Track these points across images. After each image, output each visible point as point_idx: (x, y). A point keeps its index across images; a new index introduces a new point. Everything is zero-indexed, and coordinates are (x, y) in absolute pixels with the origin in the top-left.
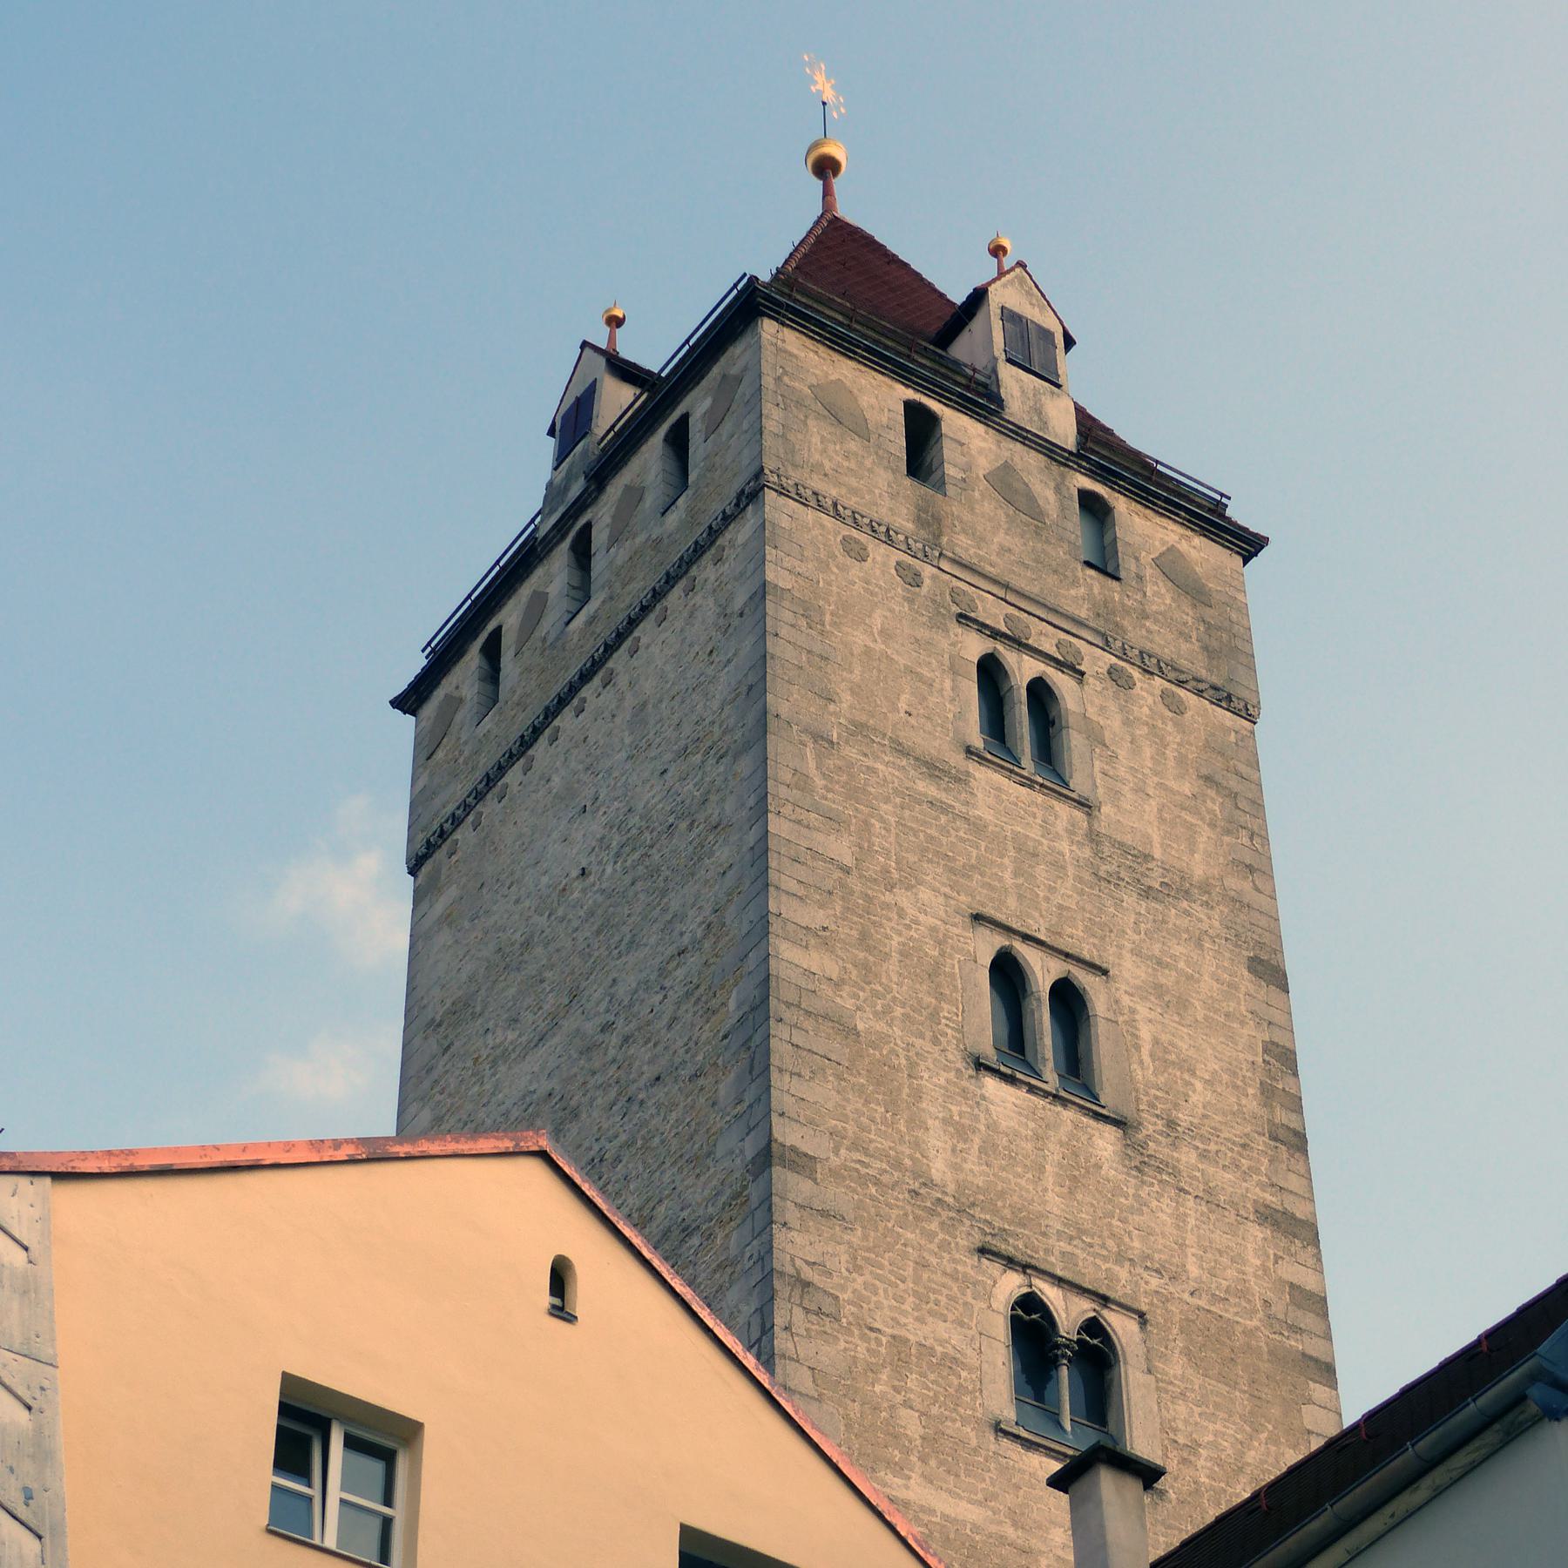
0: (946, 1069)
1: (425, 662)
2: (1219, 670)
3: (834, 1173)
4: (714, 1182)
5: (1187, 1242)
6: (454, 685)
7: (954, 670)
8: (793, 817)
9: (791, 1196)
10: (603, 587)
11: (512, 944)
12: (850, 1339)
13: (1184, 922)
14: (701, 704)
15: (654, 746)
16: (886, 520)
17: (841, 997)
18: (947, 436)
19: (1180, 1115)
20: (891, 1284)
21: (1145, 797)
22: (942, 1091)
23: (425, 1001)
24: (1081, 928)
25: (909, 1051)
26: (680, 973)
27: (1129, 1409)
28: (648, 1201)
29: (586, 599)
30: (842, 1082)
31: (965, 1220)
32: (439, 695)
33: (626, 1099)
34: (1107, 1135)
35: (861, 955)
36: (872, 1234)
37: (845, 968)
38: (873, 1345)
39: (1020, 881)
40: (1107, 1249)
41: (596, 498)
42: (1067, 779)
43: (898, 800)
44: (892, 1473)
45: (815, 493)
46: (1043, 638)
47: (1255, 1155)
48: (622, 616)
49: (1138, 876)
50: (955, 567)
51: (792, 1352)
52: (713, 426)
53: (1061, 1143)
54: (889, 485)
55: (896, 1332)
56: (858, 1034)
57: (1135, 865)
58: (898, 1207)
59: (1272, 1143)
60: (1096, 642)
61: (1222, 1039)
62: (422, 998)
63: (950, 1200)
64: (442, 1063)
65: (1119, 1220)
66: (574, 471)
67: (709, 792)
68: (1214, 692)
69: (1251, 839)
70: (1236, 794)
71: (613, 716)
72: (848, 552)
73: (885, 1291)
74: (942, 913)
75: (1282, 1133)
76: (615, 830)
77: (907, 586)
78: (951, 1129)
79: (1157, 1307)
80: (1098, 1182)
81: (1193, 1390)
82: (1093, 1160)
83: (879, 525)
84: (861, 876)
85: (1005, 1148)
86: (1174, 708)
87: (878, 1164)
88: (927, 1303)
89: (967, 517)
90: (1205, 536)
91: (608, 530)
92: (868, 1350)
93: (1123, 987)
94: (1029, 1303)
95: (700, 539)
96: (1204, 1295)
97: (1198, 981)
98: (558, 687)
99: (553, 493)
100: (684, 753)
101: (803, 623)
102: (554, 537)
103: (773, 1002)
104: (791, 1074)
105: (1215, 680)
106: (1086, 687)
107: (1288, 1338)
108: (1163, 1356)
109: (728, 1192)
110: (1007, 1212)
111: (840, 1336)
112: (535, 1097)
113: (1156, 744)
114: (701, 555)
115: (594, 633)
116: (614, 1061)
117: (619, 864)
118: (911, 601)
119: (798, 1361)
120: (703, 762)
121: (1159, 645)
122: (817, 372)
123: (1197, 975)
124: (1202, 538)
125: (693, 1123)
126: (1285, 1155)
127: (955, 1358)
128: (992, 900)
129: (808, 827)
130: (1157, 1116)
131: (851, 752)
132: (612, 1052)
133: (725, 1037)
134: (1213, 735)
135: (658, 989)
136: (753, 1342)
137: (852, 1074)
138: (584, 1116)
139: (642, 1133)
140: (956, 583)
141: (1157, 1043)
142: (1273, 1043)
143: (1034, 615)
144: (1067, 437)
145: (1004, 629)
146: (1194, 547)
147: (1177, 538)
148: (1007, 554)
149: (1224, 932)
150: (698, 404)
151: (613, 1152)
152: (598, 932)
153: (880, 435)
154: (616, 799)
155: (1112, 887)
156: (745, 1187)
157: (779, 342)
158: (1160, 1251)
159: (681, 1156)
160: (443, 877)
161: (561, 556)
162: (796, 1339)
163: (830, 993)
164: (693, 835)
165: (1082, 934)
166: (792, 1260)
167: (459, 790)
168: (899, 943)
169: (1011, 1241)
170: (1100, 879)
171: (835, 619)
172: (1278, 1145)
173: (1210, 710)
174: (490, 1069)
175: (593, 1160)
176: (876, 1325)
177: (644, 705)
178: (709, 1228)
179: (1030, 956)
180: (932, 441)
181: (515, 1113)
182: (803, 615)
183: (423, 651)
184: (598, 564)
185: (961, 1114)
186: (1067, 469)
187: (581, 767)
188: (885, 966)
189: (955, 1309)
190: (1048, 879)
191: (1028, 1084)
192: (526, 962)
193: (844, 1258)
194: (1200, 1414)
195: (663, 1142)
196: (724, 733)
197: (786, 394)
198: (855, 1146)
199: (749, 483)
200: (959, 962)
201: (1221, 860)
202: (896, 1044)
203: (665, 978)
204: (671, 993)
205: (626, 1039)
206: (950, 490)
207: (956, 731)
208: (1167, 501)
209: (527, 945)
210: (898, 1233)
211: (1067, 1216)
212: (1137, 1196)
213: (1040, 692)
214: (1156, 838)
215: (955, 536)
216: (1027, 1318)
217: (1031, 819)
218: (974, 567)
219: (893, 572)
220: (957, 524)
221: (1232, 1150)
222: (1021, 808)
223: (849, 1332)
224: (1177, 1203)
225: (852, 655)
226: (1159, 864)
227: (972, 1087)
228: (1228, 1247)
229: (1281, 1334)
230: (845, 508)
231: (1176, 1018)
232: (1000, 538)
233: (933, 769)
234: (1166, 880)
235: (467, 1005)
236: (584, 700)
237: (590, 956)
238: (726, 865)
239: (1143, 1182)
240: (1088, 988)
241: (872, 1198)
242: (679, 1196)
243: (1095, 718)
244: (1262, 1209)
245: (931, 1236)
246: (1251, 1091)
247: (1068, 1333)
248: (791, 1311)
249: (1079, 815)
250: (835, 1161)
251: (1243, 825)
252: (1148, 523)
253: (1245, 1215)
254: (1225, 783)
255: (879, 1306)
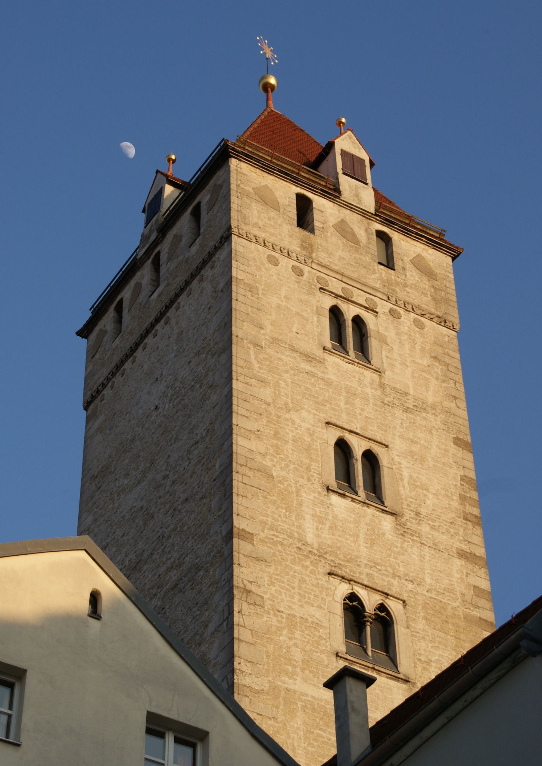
0: (314, 492)
1: (90, 315)
2: (440, 308)
3: (262, 541)
4: (210, 546)
5: (425, 568)
6: (103, 325)
7: (318, 313)
8: (244, 381)
9: (242, 552)
10: (165, 280)
11: (127, 440)
12: (269, 616)
13: (424, 423)
14: (206, 331)
15: (186, 350)
16: (287, 247)
17: (265, 461)
18: (315, 208)
19: (422, 510)
20: (288, 590)
21: (405, 367)
22: (312, 502)
23: (90, 467)
24: (376, 427)
25: (296, 484)
26: (196, 452)
27: (398, 645)
28: (182, 555)
29: (157, 286)
30: (266, 500)
31: (322, 560)
32: (97, 329)
33: (173, 509)
34: (388, 519)
35: (275, 442)
36: (279, 568)
37: (267, 448)
38: (280, 619)
39: (348, 406)
40: (388, 572)
41: (162, 241)
42: (370, 360)
43: (292, 372)
44: (288, 677)
45: (255, 236)
46: (359, 297)
47: (457, 527)
48: (173, 293)
49: (402, 402)
50: (319, 266)
51: (242, 623)
52: (211, 207)
53: (367, 524)
54: (289, 232)
55: (290, 612)
56: (273, 478)
57: (401, 398)
58: (291, 555)
59: (465, 521)
60: (383, 298)
61: (442, 475)
62: (89, 465)
63: (315, 551)
64: (97, 494)
65: (394, 558)
66: (153, 228)
67: (208, 371)
68: (438, 318)
69: (455, 384)
70: (448, 364)
71: (169, 337)
72: (270, 262)
73: (285, 593)
74: (312, 422)
75: (470, 517)
76: (169, 388)
77: (298, 276)
78: (316, 519)
79: (411, 597)
80: (384, 541)
81: (428, 636)
82: (381, 532)
83: (284, 249)
84: (275, 406)
85: (341, 527)
86: (419, 326)
87: (282, 536)
88: (305, 598)
89: (324, 244)
90: (434, 249)
91: (167, 255)
92: (277, 621)
93: (396, 453)
94: (353, 597)
95: (205, 258)
96: (433, 592)
97: (430, 449)
98: (146, 325)
99: (144, 238)
100: (198, 353)
101: (249, 294)
102: (144, 258)
103: (234, 464)
104: (243, 496)
105: (438, 313)
106: (379, 319)
107: (473, 611)
108: (414, 620)
109: (215, 550)
110: (341, 556)
111: (264, 614)
112: (135, 509)
113: (411, 342)
114: (206, 265)
115: (161, 300)
116: (168, 492)
117: (171, 404)
118: (298, 283)
119: (245, 627)
120: (206, 357)
121: (413, 299)
122: (255, 182)
123: (429, 446)
124: (433, 250)
125: (201, 520)
126: (471, 527)
127: (317, 624)
128: (335, 415)
129: (251, 385)
130: (411, 510)
131: (271, 351)
132: (167, 488)
133: (214, 480)
134: (438, 338)
135: (186, 459)
136: (225, 619)
137: (270, 496)
138: (156, 517)
139: (179, 524)
140: (319, 274)
141: (411, 478)
142: (465, 476)
143: (355, 287)
144: (370, 207)
145: (341, 294)
146: (429, 254)
147: (421, 250)
148: (343, 260)
149: (442, 427)
150: (204, 197)
151: (168, 533)
152: (162, 434)
153: (285, 209)
154: (170, 375)
155: (390, 408)
156: (222, 548)
157: (239, 169)
158: (413, 572)
159: (196, 534)
160: (98, 411)
161: (148, 266)
162: (244, 617)
163: (261, 460)
164: (202, 390)
165: (376, 429)
166: (242, 581)
167: (105, 372)
168: (292, 436)
169: (343, 569)
170: (385, 404)
171: (264, 292)
172: (468, 522)
173: (436, 327)
174: (117, 496)
175: (159, 537)
176: (281, 609)
177: (182, 332)
178: (207, 567)
179: (352, 440)
180: (309, 211)
181: (127, 516)
182: (249, 291)
183: (90, 310)
184: (163, 270)
185: (320, 512)
186: (370, 221)
187: (156, 360)
188: (286, 446)
189: (318, 601)
190: (361, 405)
191: (351, 498)
192: (132, 448)
193: (266, 579)
194: (432, 647)
195: (188, 528)
196: (215, 344)
197: (242, 192)
198: (271, 529)
199: (225, 232)
200: (320, 444)
201: (441, 394)
202: (290, 481)
203: (190, 454)
204: (192, 461)
205: (174, 482)
206: (316, 232)
207: (319, 340)
208: (416, 234)
209: (133, 440)
210: (291, 567)
211: (370, 557)
212: (402, 547)
213: (358, 321)
214: (411, 385)
215: (319, 253)
216: (351, 604)
217: (353, 379)
218: (327, 267)
219: (291, 270)
220: (320, 248)
221: (446, 525)
222: (349, 374)
223: (269, 613)
224: (421, 549)
225: (271, 307)
226: (412, 397)
227: (326, 500)
228: (445, 570)
229: (470, 609)
230: (268, 242)
231: (420, 466)
232: (340, 253)
233: (309, 358)
234: (415, 404)
235: (108, 468)
236: (157, 331)
237: (159, 445)
238: (215, 403)
239: (404, 541)
240: (379, 454)
241: (280, 551)
242: (195, 552)
243: (383, 332)
244: (460, 552)
245: (306, 567)
246: (455, 498)
247: (370, 611)
248: (241, 604)
249: (375, 376)
250: (262, 535)
251: (451, 378)
252: (408, 244)
253: (452, 555)
254: (443, 360)
255: (282, 600)
